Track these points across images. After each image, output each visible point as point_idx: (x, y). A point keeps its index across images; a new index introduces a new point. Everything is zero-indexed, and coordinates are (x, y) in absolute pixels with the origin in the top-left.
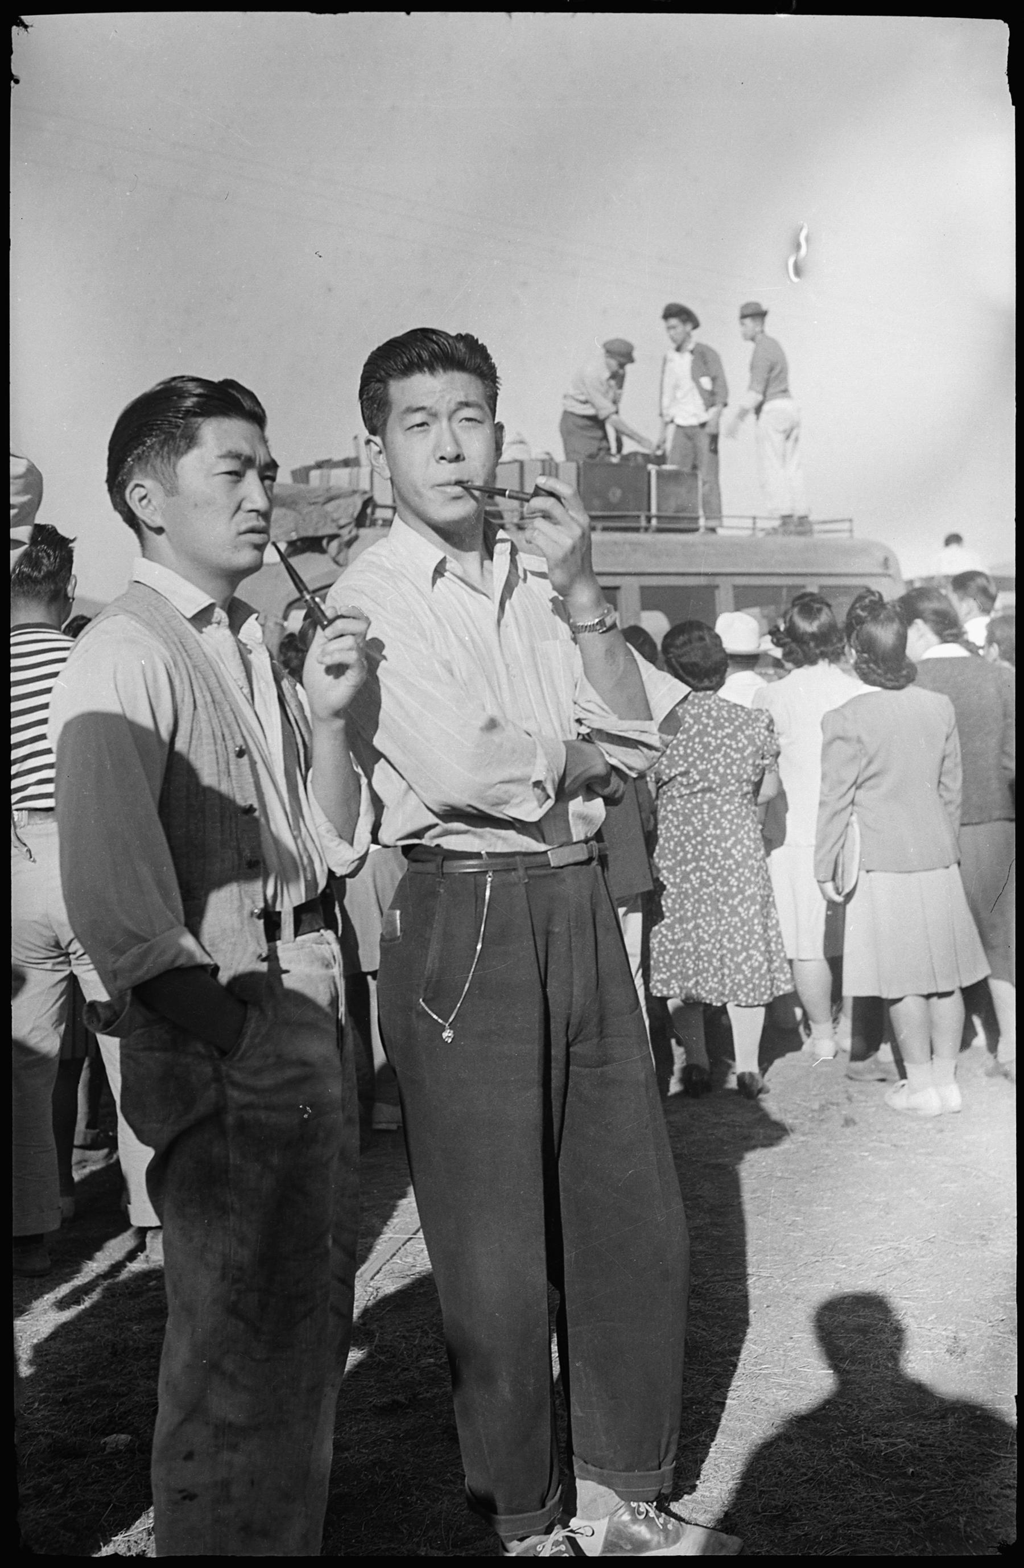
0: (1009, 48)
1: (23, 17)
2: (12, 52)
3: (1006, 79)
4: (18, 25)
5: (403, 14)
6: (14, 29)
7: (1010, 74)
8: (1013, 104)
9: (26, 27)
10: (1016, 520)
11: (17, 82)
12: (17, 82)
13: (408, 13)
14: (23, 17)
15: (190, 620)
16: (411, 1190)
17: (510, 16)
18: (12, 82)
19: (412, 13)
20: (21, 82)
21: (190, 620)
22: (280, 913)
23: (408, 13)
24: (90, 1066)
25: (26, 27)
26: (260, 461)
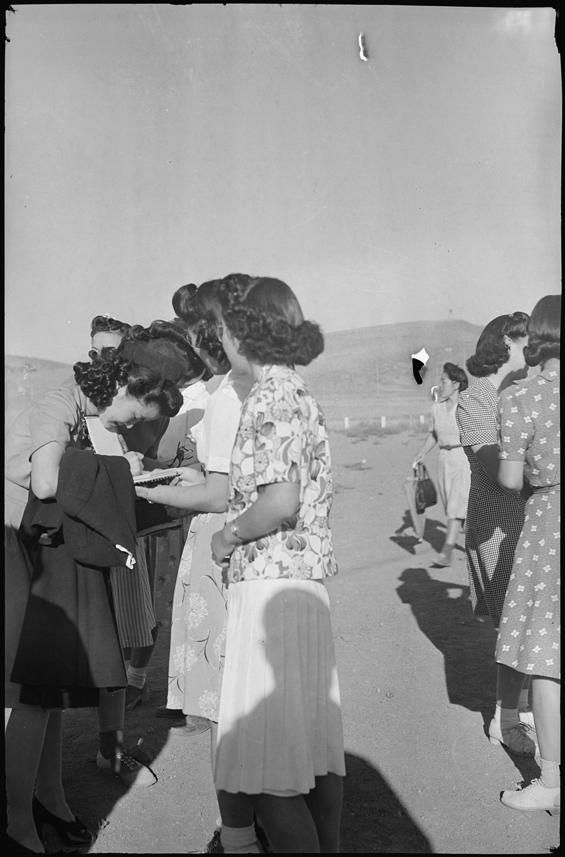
4: (9, 10)
5: (222, 5)
9: (14, 11)
11: (9, 41)
12: (9, 41)
13: (225, 4)
17: (281, 6)
18: (6, 41)
19: (227, 4)
20: (11, 41)
23: (225, 4)
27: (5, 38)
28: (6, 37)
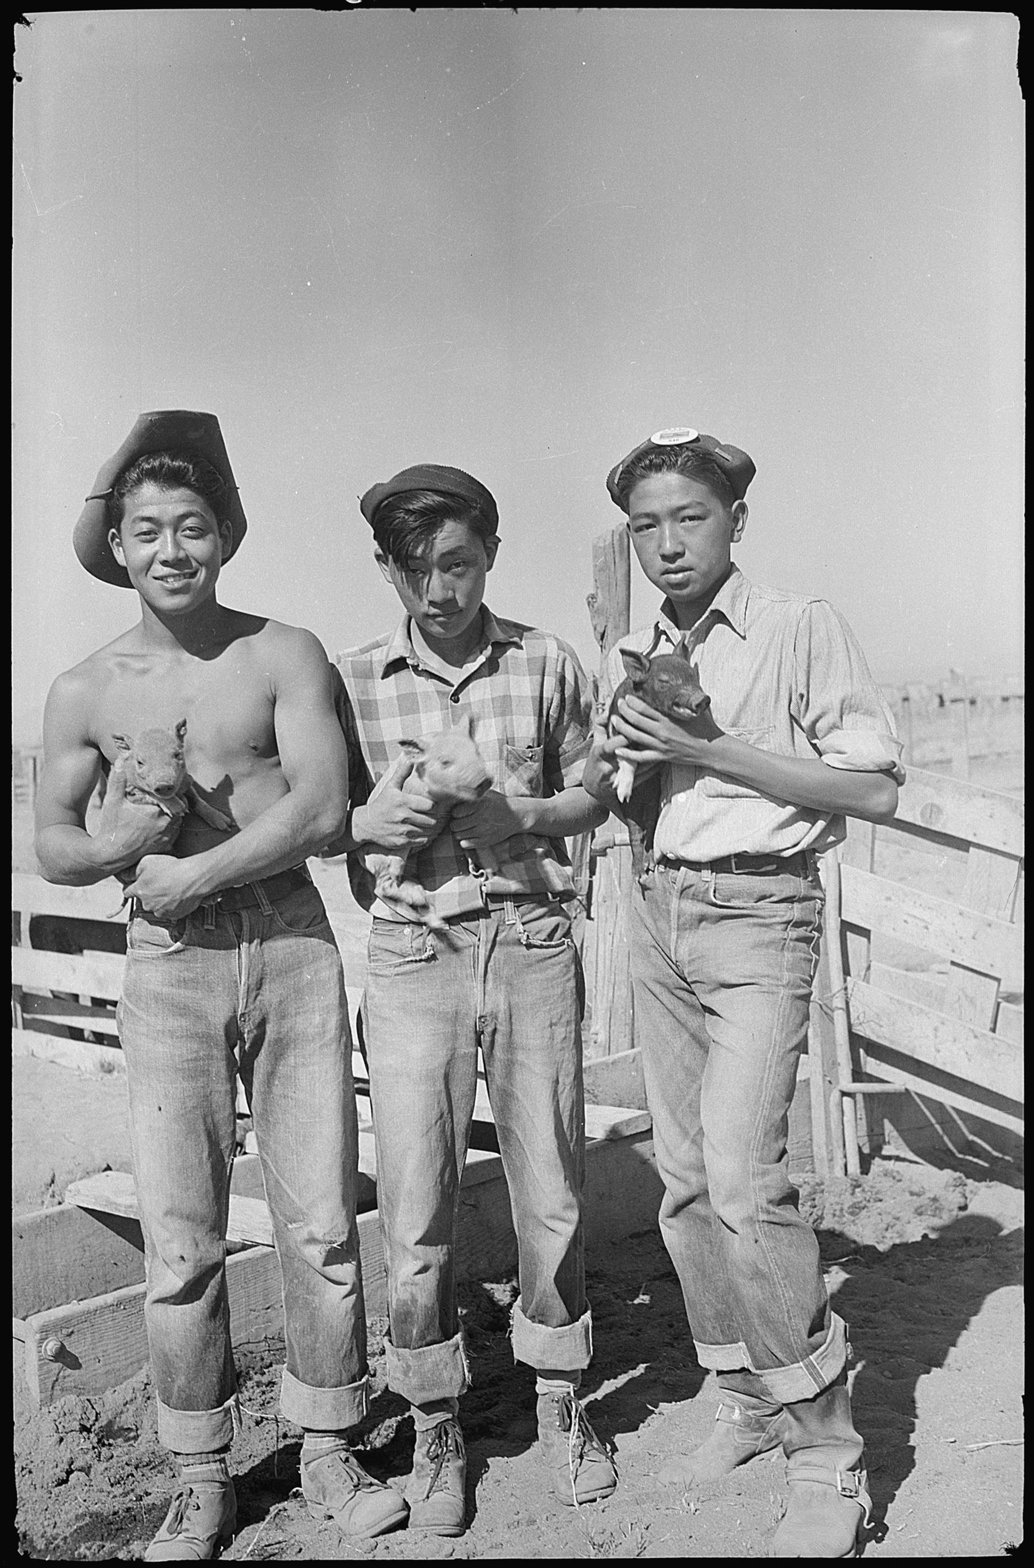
0: (1020, 41)
1: (24, 14)
2: (14, 50)
3: (1017, 71)
4: (21, 23)
6: (17, 25)
7: (1021, 65)
8: (1023, 98)
9: (28, 24)
10: (1026, 515)
12: (19, 79)
13: (413, 10)
14: (24, 14)
15: (368, 1095)
16: (487, 1286)
18: (15, 79)
19: (418, 10)
21: (368, 1095)
22: (913, 1448)
23: (413, 10)
24: (416, 832)
25: (28, 24)
26: (345, 1444)
28: (15, 73)
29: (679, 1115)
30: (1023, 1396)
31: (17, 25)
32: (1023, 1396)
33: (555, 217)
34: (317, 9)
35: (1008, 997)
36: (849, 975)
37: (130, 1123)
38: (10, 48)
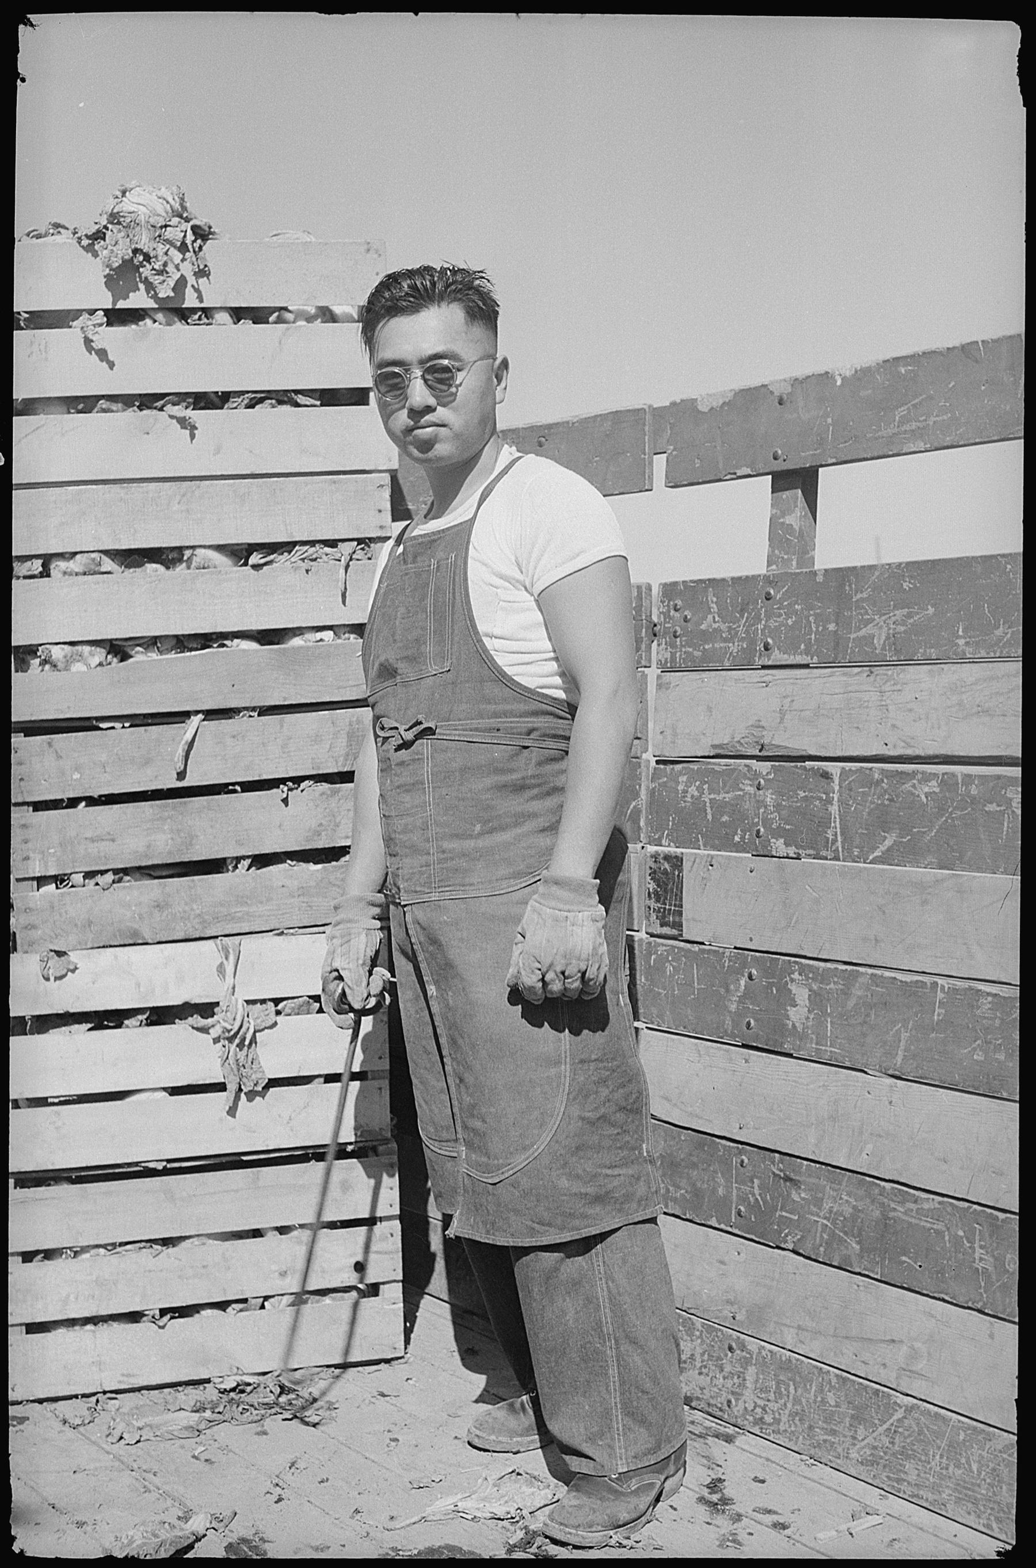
1: (29, 16)
2: (18, 51)
4: (26, 25)
6: (21, 27)
7: (1022, 73)
8: (1024, 106)
9: (32, 25)
11: (23, 80)
12: (23, 80)
13: (416, 14)
14: (29, 16)
23: (416, 14)
25: (32, 25)
27: (17, 75)
28: (19, 74)
29: (969, 652)
30: (1016, 1400)
31: (21, 27)
32: (1016, 1400)
33: (733, 1007)
34: (320, 13)
35: (221, 973)
36: (326, 1082)
37: (247, 1043)
38: (14, 49)
